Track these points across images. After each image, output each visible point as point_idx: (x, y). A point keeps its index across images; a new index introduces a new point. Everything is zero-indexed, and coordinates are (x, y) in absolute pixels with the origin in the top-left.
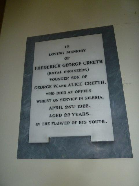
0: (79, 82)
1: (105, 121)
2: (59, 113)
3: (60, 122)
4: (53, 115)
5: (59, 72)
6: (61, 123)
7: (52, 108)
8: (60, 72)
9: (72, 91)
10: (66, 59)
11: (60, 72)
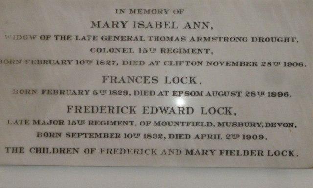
0: (143, 75)
1: (289, 94)
2: (150, 105)
3: (161, 108)
4: (157, 112)
5: (139, 38)
6: (163, 109)
7: (200, 137)
8: (141, 37)
9: (166, 92)
10: (143, 123)
11: (141, 37)
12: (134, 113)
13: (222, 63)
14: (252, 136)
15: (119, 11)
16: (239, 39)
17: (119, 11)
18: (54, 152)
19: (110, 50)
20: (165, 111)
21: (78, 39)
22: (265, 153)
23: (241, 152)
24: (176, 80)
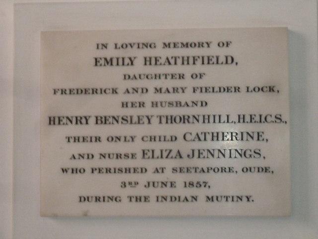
12: (116, 93)
17: (100, 46)
18: (220, 91)
19: (254, 89)
21: (230, 121)
22: (243, 89)
23: (217, 89)
24: (257, 90)
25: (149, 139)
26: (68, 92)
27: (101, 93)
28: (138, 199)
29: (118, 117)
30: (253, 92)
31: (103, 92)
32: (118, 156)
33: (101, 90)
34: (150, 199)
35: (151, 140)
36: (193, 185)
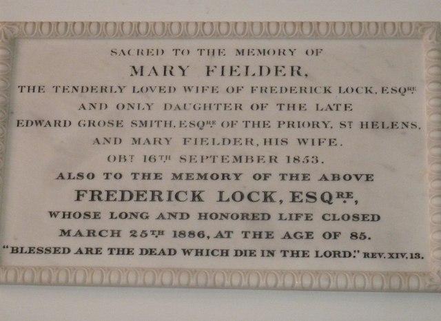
13: (359, 176)
14: (246, 199)
15: (266, 253)
16: (224, 216)
17: (266, 253)
20: (304, 142)
25: (220, 253)
26: (94, 251)
27: (208, 255)
28: (121, 251)
29: (137, 213)
30: (324, 257)
31: (210, 254)
32: (199, 253)
33: (245, 255)
34: (310, 254)
35: (222, 255)
36: (356, 236)
